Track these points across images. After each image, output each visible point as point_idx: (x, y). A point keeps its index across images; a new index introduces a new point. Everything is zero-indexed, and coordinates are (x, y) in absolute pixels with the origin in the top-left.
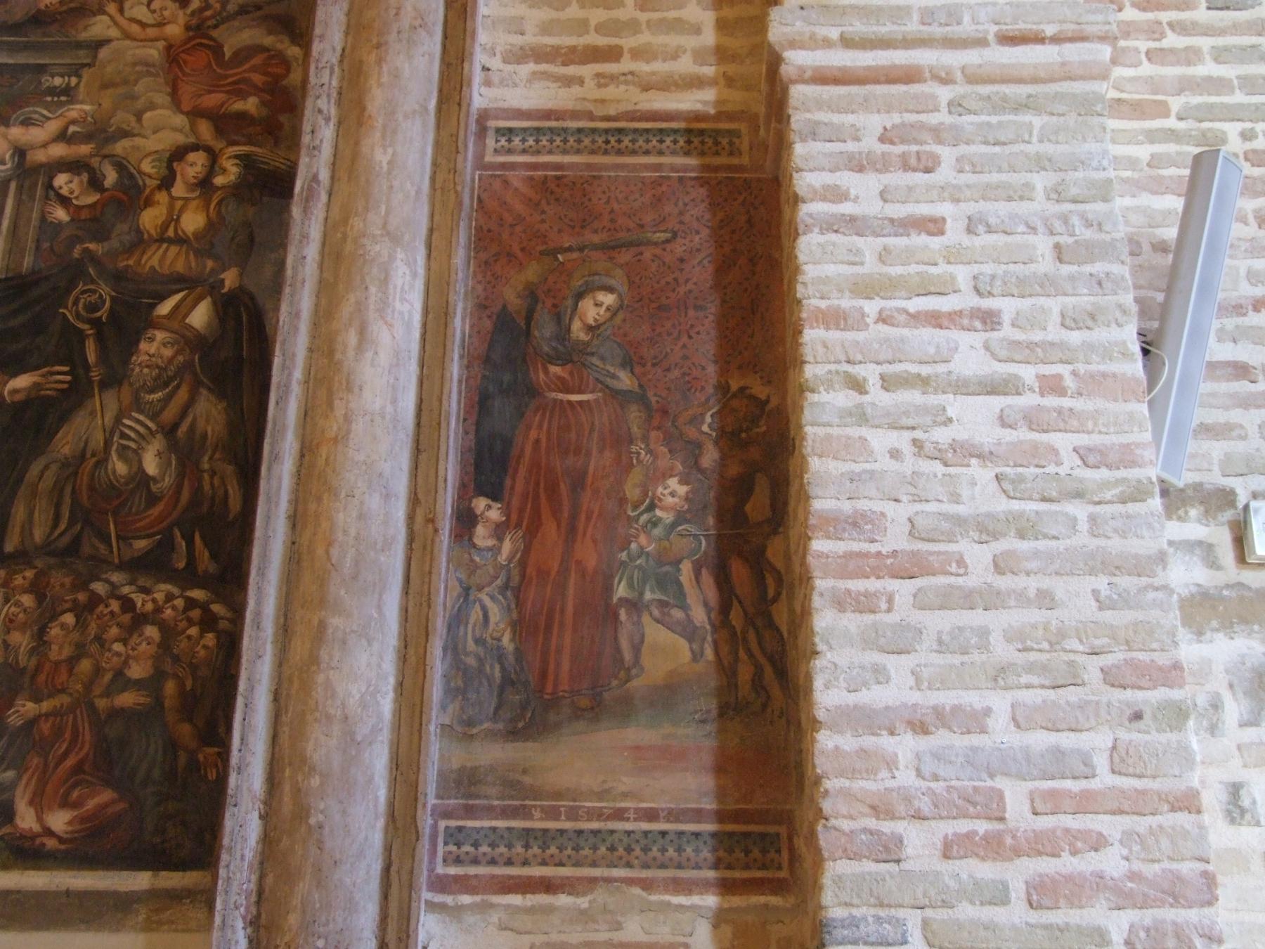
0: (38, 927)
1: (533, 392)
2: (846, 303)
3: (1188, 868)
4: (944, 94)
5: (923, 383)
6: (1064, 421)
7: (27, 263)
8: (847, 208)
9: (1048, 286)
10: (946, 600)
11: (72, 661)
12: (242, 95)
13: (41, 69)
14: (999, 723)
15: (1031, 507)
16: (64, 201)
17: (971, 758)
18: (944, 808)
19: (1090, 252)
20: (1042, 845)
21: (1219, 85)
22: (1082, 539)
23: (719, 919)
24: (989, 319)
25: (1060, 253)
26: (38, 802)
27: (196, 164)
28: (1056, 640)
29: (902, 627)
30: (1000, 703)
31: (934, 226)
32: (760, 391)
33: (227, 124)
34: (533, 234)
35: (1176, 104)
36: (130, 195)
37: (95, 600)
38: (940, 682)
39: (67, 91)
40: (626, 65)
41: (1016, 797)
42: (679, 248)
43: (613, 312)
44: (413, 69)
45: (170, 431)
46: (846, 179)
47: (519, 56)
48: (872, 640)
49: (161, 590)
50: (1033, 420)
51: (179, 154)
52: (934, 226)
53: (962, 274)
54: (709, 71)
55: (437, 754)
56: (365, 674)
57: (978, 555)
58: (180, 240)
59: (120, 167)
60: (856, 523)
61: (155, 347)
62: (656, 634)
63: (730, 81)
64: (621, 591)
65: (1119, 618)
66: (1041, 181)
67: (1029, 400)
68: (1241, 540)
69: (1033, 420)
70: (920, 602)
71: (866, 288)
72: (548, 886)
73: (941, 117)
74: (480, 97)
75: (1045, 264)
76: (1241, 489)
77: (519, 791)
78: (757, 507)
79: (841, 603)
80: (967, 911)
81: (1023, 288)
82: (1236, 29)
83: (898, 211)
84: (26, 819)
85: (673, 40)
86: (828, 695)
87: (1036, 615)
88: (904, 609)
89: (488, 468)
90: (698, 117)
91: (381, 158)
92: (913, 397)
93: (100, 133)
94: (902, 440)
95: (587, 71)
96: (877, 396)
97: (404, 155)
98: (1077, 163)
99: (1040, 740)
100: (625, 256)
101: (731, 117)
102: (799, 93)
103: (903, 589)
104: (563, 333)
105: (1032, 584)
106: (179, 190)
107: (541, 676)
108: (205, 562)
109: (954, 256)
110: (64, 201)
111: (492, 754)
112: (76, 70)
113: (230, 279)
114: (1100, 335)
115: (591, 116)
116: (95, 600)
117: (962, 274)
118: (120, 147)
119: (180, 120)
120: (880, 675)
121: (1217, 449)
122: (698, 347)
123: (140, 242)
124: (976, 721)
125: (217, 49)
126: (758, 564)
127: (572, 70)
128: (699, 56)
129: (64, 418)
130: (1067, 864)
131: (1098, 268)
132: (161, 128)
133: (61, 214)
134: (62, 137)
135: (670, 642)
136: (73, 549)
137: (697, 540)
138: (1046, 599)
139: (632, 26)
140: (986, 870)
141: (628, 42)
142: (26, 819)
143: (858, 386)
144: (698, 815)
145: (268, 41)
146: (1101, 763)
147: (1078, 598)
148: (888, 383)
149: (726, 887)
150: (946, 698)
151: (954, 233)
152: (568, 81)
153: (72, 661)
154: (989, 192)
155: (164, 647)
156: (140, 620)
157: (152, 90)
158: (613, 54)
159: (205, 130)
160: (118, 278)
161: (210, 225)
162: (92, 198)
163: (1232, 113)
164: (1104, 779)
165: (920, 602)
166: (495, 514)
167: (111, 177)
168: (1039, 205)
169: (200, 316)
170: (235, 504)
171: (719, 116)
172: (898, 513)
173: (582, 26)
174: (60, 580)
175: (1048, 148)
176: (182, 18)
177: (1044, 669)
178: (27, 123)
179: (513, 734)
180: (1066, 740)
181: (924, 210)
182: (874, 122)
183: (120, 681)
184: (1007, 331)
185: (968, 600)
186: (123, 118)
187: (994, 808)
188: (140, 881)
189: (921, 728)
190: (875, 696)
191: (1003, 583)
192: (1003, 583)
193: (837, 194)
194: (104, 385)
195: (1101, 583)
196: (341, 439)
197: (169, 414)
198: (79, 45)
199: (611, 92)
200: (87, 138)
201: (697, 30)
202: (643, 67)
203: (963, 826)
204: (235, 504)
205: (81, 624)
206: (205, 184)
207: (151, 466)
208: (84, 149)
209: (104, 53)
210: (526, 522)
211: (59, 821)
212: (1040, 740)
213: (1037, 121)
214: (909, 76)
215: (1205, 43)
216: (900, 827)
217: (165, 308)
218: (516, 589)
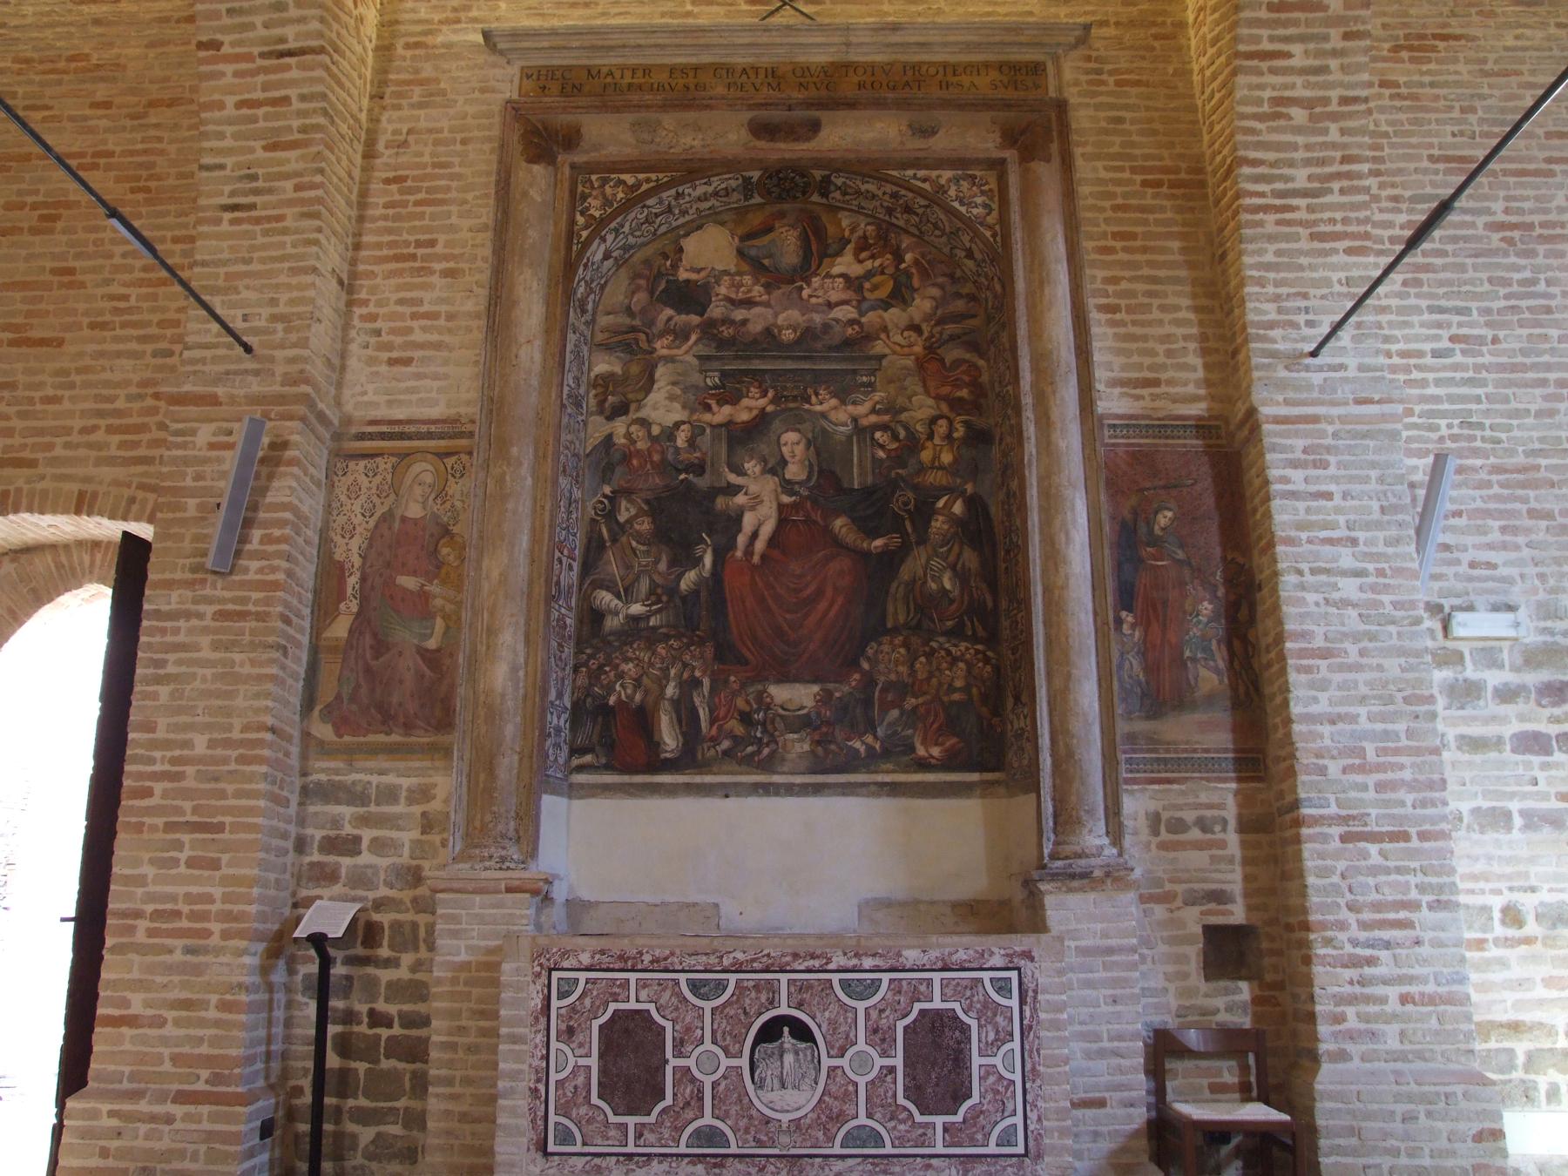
0: (935, 797)
1: (1141, 560)
2: (1293, 533)
3: (1436, 777)
4: (1330, 429)
5: (1327, 571)
6: (1386, 588)
7: (870, 480)
8: (1289, 487)
9: (1378, 525)
10: (1342, 668)
11: (929, 679)
12: (959, 388)
13: (855, 372)
14: (1363, 719)
15: (1374, 628)
16: (882, 447)
17: (1353, 734)
18: (1342, 753)
19: (1396, 509)
20: (1380, 768)
21: (1436, 399)
22: (1395, 641)
23: (1237, 793)
24: (1354, 542)
25: (1383, 510)
26: (924, 742)
27: (942, 427)
28: (1385, 685)
29: (1324, 680)
30: (1362, 711)
31: (1328, 496)
32: (1241, 560)
33: (956, 404)
34: (1133, 478)
35: (1417, 409)
36: (913, 445)
37: (933, 651)
38: (1341, 702)
39: (870, 384)
40: (1163, 389)
41: (1370, 749)
42: (1198, 487)
43: (1172, 520)
44: (1068, 395)
45: (953, 567)
46: (1289, 472)
47: (1114, 383)
48: (1312, 685)
49: (963, 646)
50: (1374, 588)
51: (933, 421)
52: (1328, 496)
53: (1342, 519)
54: (1202, 392)
55: (1122, 727)
56: (1087, 695)
57: (1352, 649)
58: (941, 468)
59: (906, 428)
60: (1304, 635)
61: (938, 524)
62: (1203, 672)
63: (1213, 398)
64: (1187, 654)
65: (1410, 676)
66: (1374, 474)
67: (1371, 580)
68: (1446, 629)
69: (1374, 588)
70: (1330, 668)
71: (1301, 526)
72: (1169, 781)
73: (1329, 441)
74: (1102, 407)
75: (1376, 515)
76: (1447, 604)
77: (1153, 741)
78: (1243, 614)
79: (1299, 670)
80: (1353, 794)
81: (1368, 526)
82: (1444, 368)
83: (1313, 488)
84: (921, 751)
85: (1183, 375)
86: (1296, 709)
87: (1375, 675)
88: (1324, 673)
89: (1126, 597)
90: (1200, 418)
91: (1062, 444)
92: (1323, 578)
93: (892, 409)
94: (1318, 597)
95: (1145, 392)
96: (1308, 578)
97: (1070, 440)
98: (1389, 465)
99: (1379, 726)
100: (1174, 492)
101: (1216, 418)
102: (1266, 427)
103: (1323, 664)
104: (1151, 532)
105: (1374, 661)
106: (937, 441)
107: (1157, 692)
108: (981, 633)
109: (1338, 510)
110: (882, 447)
111: (1141, 726)
112: (873, 372)
113: (969, 488)
114: (1400, 549)
115: (1149, 417)
116: (933, 651)
117: (1342, 519)
118: (904, 416)
119: (930, 402)
120: (1316, 700)
121: (1436, 585)
122: (1210, 540)
123: (922, 469)
124: (1353, 719)
125: (942, 361)
126: (1244, 640)
127: (1138, 391)
128: (1197, 384)
129: (902, 561)
130: (1390, 776)
131: (1400, 517)
132: (921, 408)
133: (881, 454)
134: (873, 411)
135: (1209, 676)
136: (918, 626)
137: (1219, 629)
138: (1380, 668)
139: (1163, 367)
140: (1359, 778)
141: (1164, 376)
142: (921, 751)
143: (1300, 573)
144: (1226, 750)
145: (968, 356)
146: (1403, 736)
147: (1393, 665)
148: (1313, 572)
149: (1239, 780)
150: (1342, 710)
151: (1337, 500)
152: (1138, 398)
153: (929, 679)
154: (1352, 479)
155: (969, 671)
156: (954, 661)
157: (913, 384)
158: (1155, 383)
159: (944, 408)
160: (916, 488)
161: (956, 461)
162: (894, 446)
163: (1443, 414)
164: (1404, 742)
165: (1330, 668)
166: (1130, 619)
167: (902, 434)
168: (1373, 486)
169: (958, 508)
170: (990, 604)
171: (1210, 418)
172: (1319, 631)
173: (1140, 367)
174: (916, 641)
175: (1376, 458)
176: (920, 342)
177: (1380, 697)
178: (854, 403)
179: (1148, 718)
180: (1390, 727)
181: (1323, 488)
182: (1300, 443)
183: (951, 689)
184: (1361, 548)
185: (1351, 668)
186: (901, 401)
187: (1361, 752)
188: (974, 777)
189: (1333, 722)
190: (1314, 709)
191: (1364, 661)
192: (1364, 661)
193: (1285, 480)
194: (918, 544)
195: (1402, 660)
196: (1065, 587)
197: (951, 558)
198: (870, 358)
199: (1158, 404)
200: (886, 411)
201: (1195, 370)
202: (1171, 390)
203: (1350, 761)
204: (990, 604)
205: (929, 662)
206: (949, 437)
207: (948, 586)
208: (886, 418)
209: (885, 362)
210: (1144, 622)
211: (936, 751)
212: (1379, 726)
213: (1371, 443)
214: (1315, 419)
215: (1430, 376)
216: (1326, 762)
217: (940, 504)
218: (1145, 651)
